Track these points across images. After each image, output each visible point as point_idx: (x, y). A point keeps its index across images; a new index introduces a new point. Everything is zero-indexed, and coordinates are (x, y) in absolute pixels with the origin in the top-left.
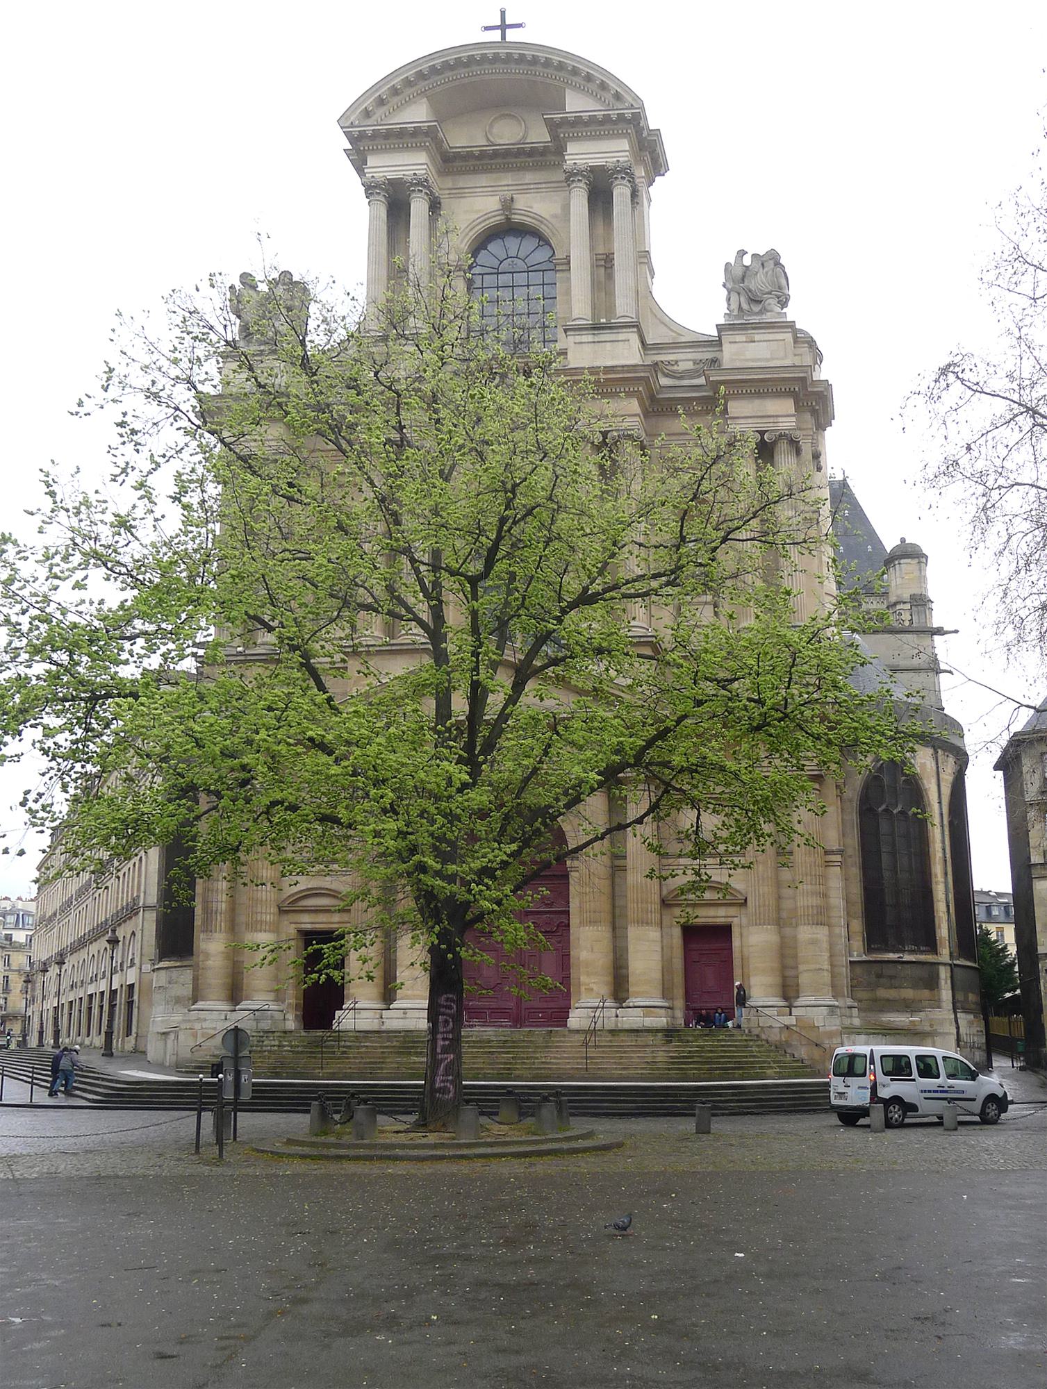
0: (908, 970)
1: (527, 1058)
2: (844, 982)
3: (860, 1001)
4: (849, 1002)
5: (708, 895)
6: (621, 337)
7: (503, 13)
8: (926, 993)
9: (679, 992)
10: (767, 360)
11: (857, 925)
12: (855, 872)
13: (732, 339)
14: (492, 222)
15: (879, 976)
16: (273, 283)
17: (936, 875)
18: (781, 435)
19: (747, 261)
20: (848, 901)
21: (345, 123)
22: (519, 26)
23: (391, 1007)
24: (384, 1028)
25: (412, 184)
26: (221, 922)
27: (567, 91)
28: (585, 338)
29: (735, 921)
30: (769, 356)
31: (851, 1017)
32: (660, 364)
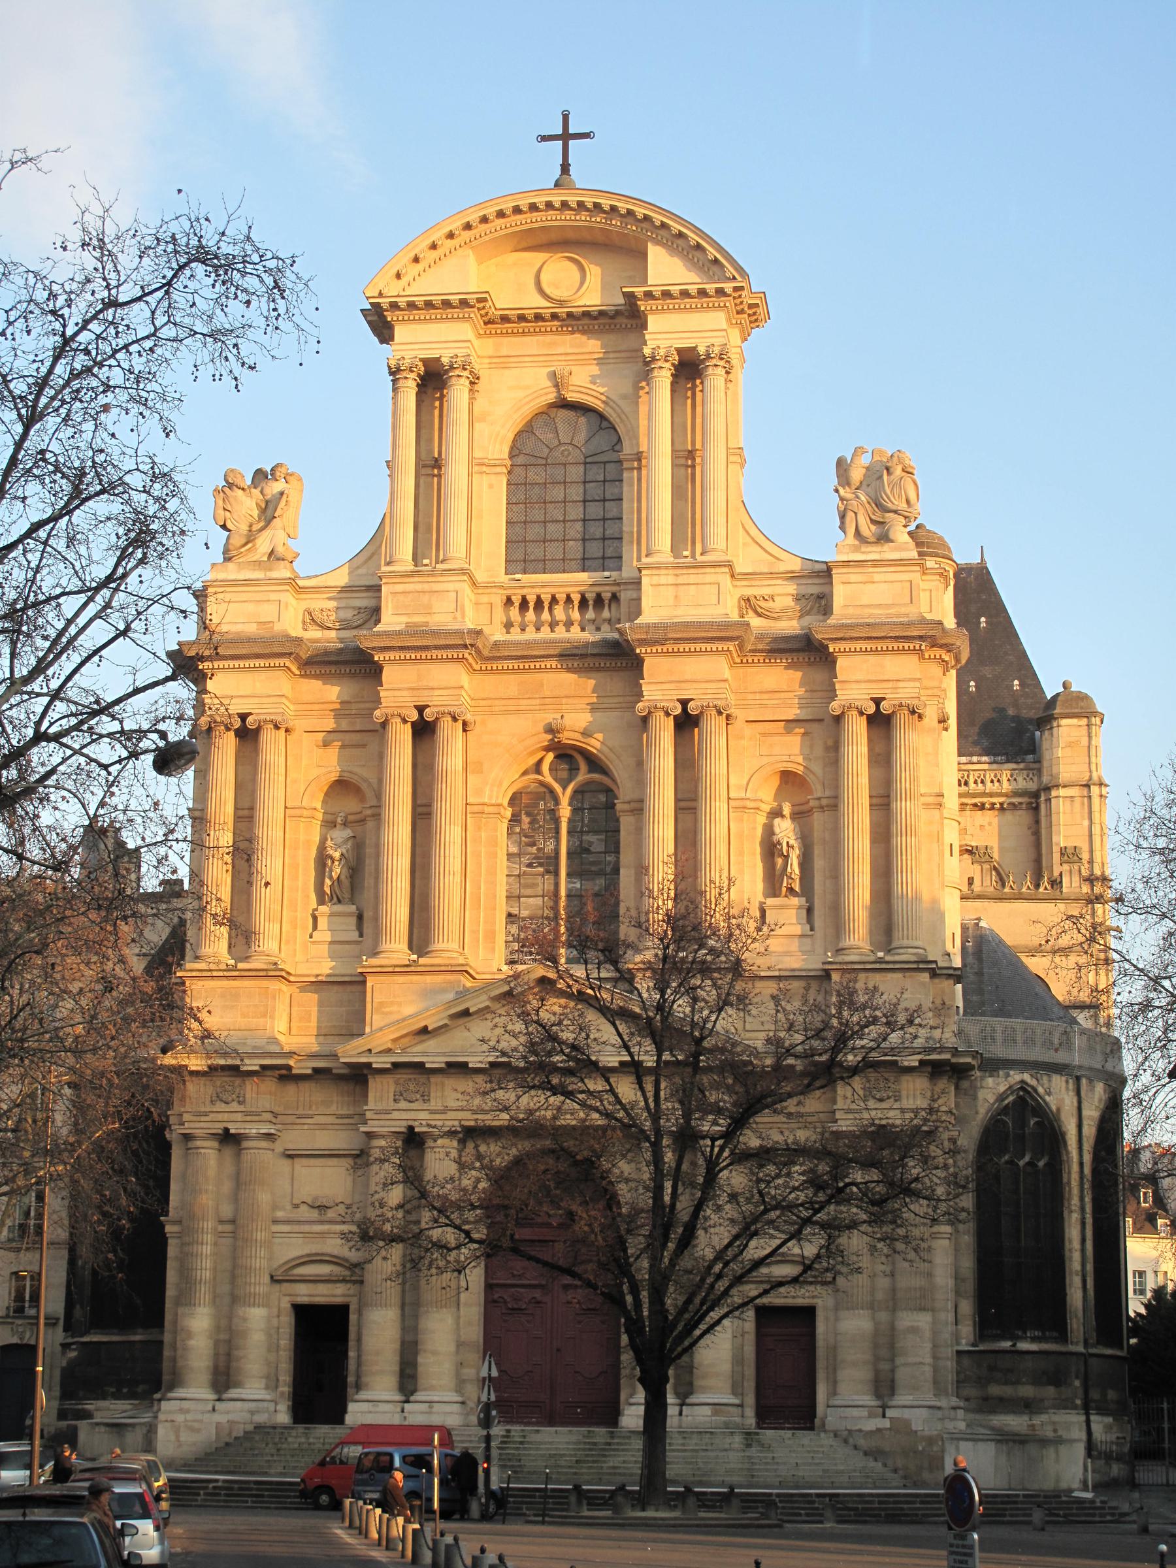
1: (594, 1462)
2: (951, 1377)
3: (967, 1400)
4: (954, 1401)
5: (668, 1186)
6: (709, 578)
7: (566, 117)
8: (1051, 1391)
9: (750, 1386)
10: (887, 606)
11: (967, 1307)
12: (968, 1239)
13: (845, 578)
17: (1070, 1241)
18: (901, 705)
20: (957, 1277)
22: (544, 138)
24: (406, 1423)
27: (650, 245)
29: (819, 1302)
30: (890, 602)
31: (955, 1419)
32: (753, 600)
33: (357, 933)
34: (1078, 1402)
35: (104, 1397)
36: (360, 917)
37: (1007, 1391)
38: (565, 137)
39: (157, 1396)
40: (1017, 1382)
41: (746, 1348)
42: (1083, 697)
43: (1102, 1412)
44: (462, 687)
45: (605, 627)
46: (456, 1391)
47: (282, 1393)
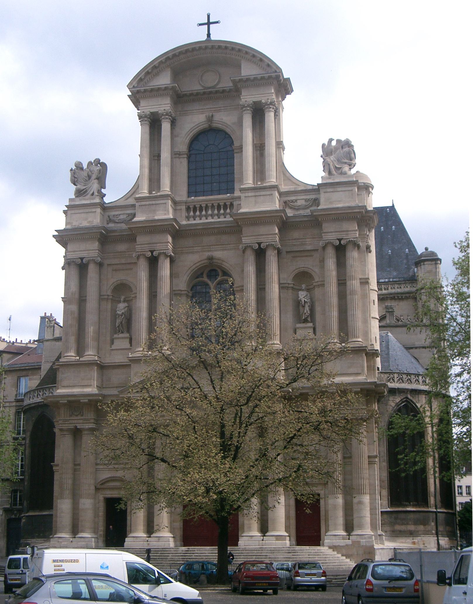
0: (412, 516)
3: (386, 532)
8: (421, 527)
13: (325, 190)
14: (201, 127)
15: (396, 518)
16: (90, 163)
19: (334, 143)
21: (130, 86)
22: (200, 25)
23: (152, 536)
25: (163, 115)
26: (67, 493)
27: (242, 61)
28: (250, 194)
32: (288, 202)
33: (129, 345)
34: (434, 532)
35: (33, 537)
36: (314, 329)
37: (403, 528)
38: (209, 23)
39: (51, 536)
40: (408, 524)
41: (291, 512)
42: (433, 254)
43: (443, 536)
44: (169, 242)
45: (228, 216)
46: (171, 532)
47: (101, 535)
